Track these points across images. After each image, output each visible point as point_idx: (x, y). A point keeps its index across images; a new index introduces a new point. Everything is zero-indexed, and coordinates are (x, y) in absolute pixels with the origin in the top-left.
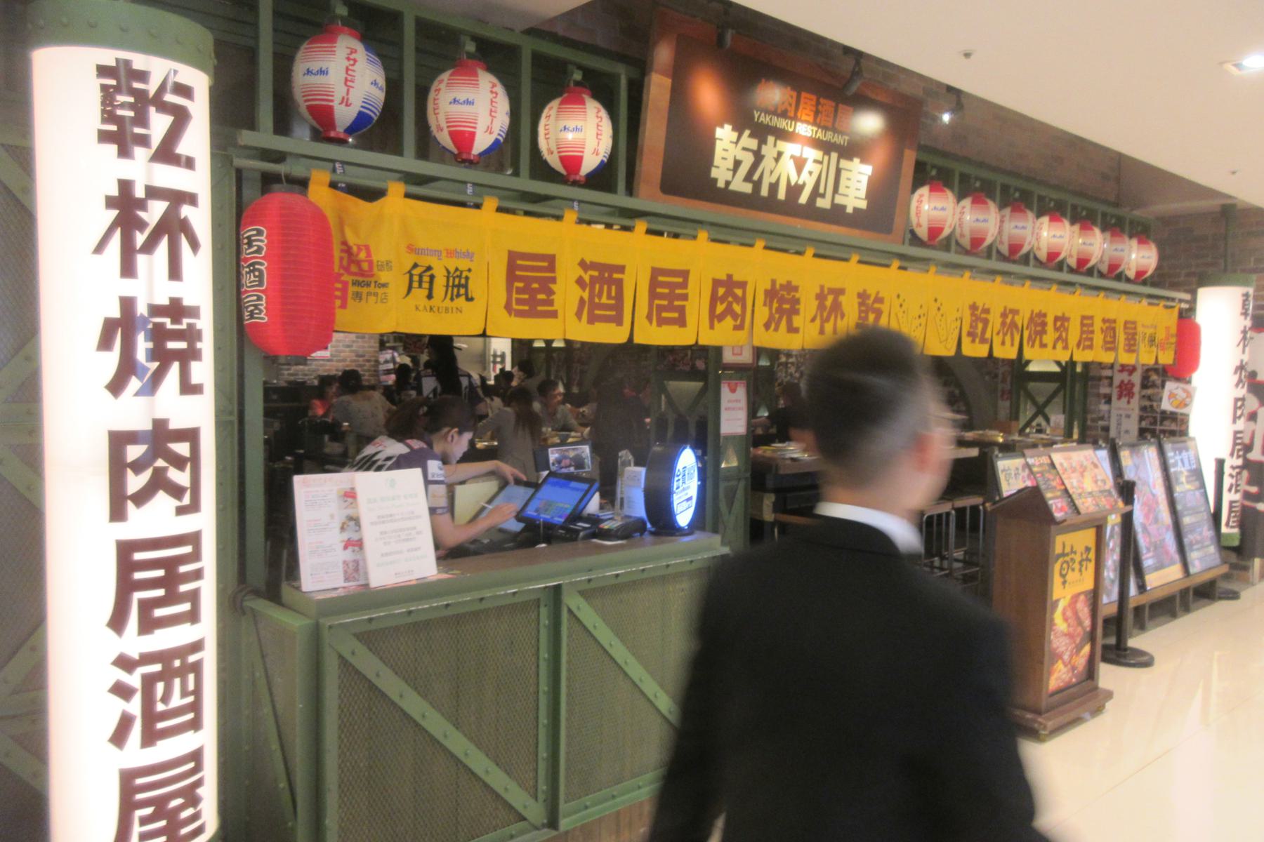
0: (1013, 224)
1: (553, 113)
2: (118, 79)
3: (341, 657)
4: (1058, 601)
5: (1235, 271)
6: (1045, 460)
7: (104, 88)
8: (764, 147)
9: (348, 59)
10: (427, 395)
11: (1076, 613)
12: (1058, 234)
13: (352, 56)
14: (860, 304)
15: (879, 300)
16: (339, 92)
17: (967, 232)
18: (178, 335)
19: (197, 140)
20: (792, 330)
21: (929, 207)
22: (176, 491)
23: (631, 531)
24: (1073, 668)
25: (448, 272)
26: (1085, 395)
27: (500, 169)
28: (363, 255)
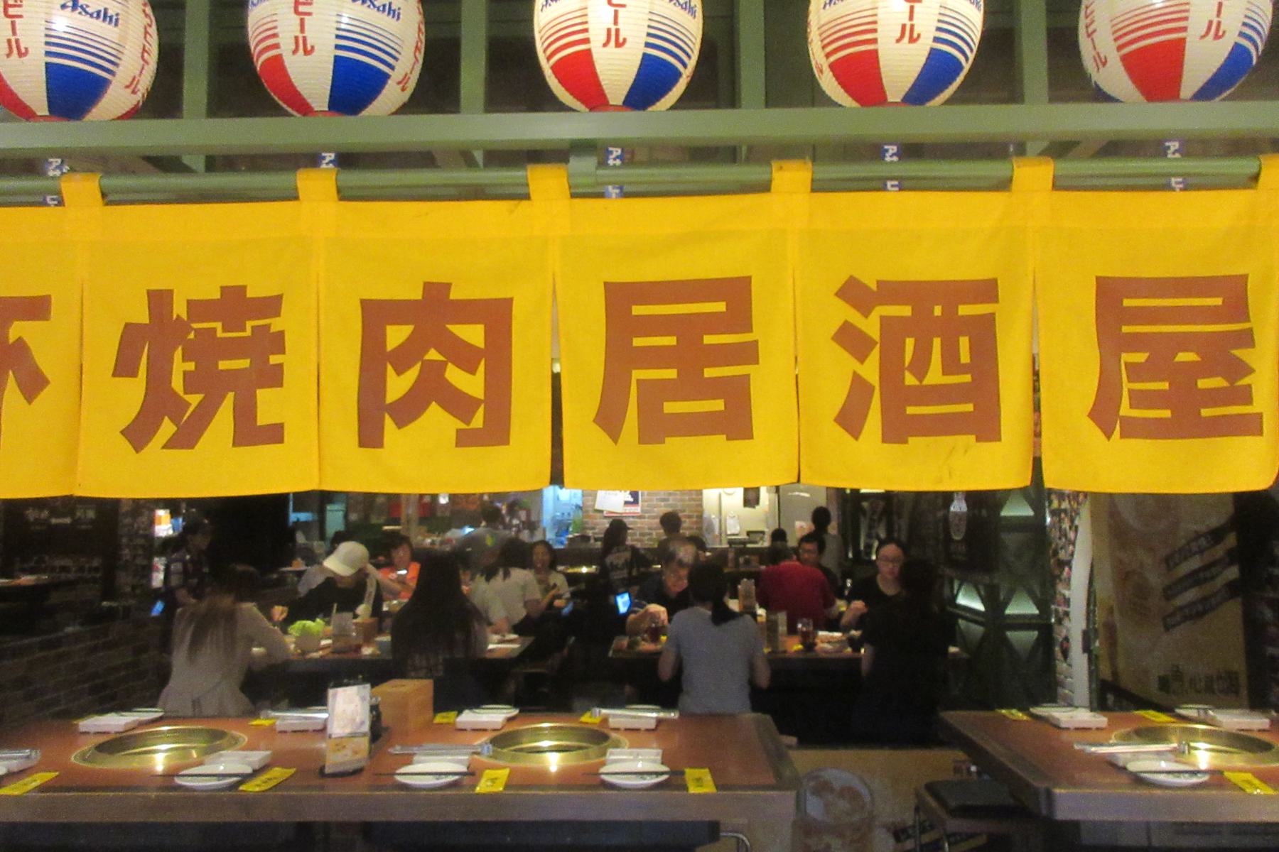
22: (458, 404)
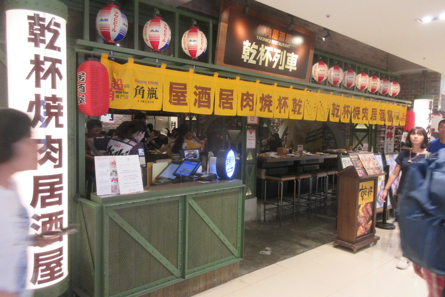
0: (348, 77)
1: (186, 35)
2: (35, 20)
3: (110, 217)
4: (360, 205)
5: (427, 94)
6: (356, 157)
7: (30, 23)
8: (260, 48)
9: (115, 16)
10: (139, 130)
11: (367, 209)
12: (364, 80)
13: (117, 15)
14: (294, 103)
15: (301, 102)
16: (112, 27)
17: (332, 78)
18: (55, 107)
19: (62, 41)
20: (270, 111)
21: (319, 70)
22: (54, 160)
23: (211, 178)
24: (366, 229)
25: (149, 89)
26: (376, 137)
27: (169, 55)
28: (119, 83)
